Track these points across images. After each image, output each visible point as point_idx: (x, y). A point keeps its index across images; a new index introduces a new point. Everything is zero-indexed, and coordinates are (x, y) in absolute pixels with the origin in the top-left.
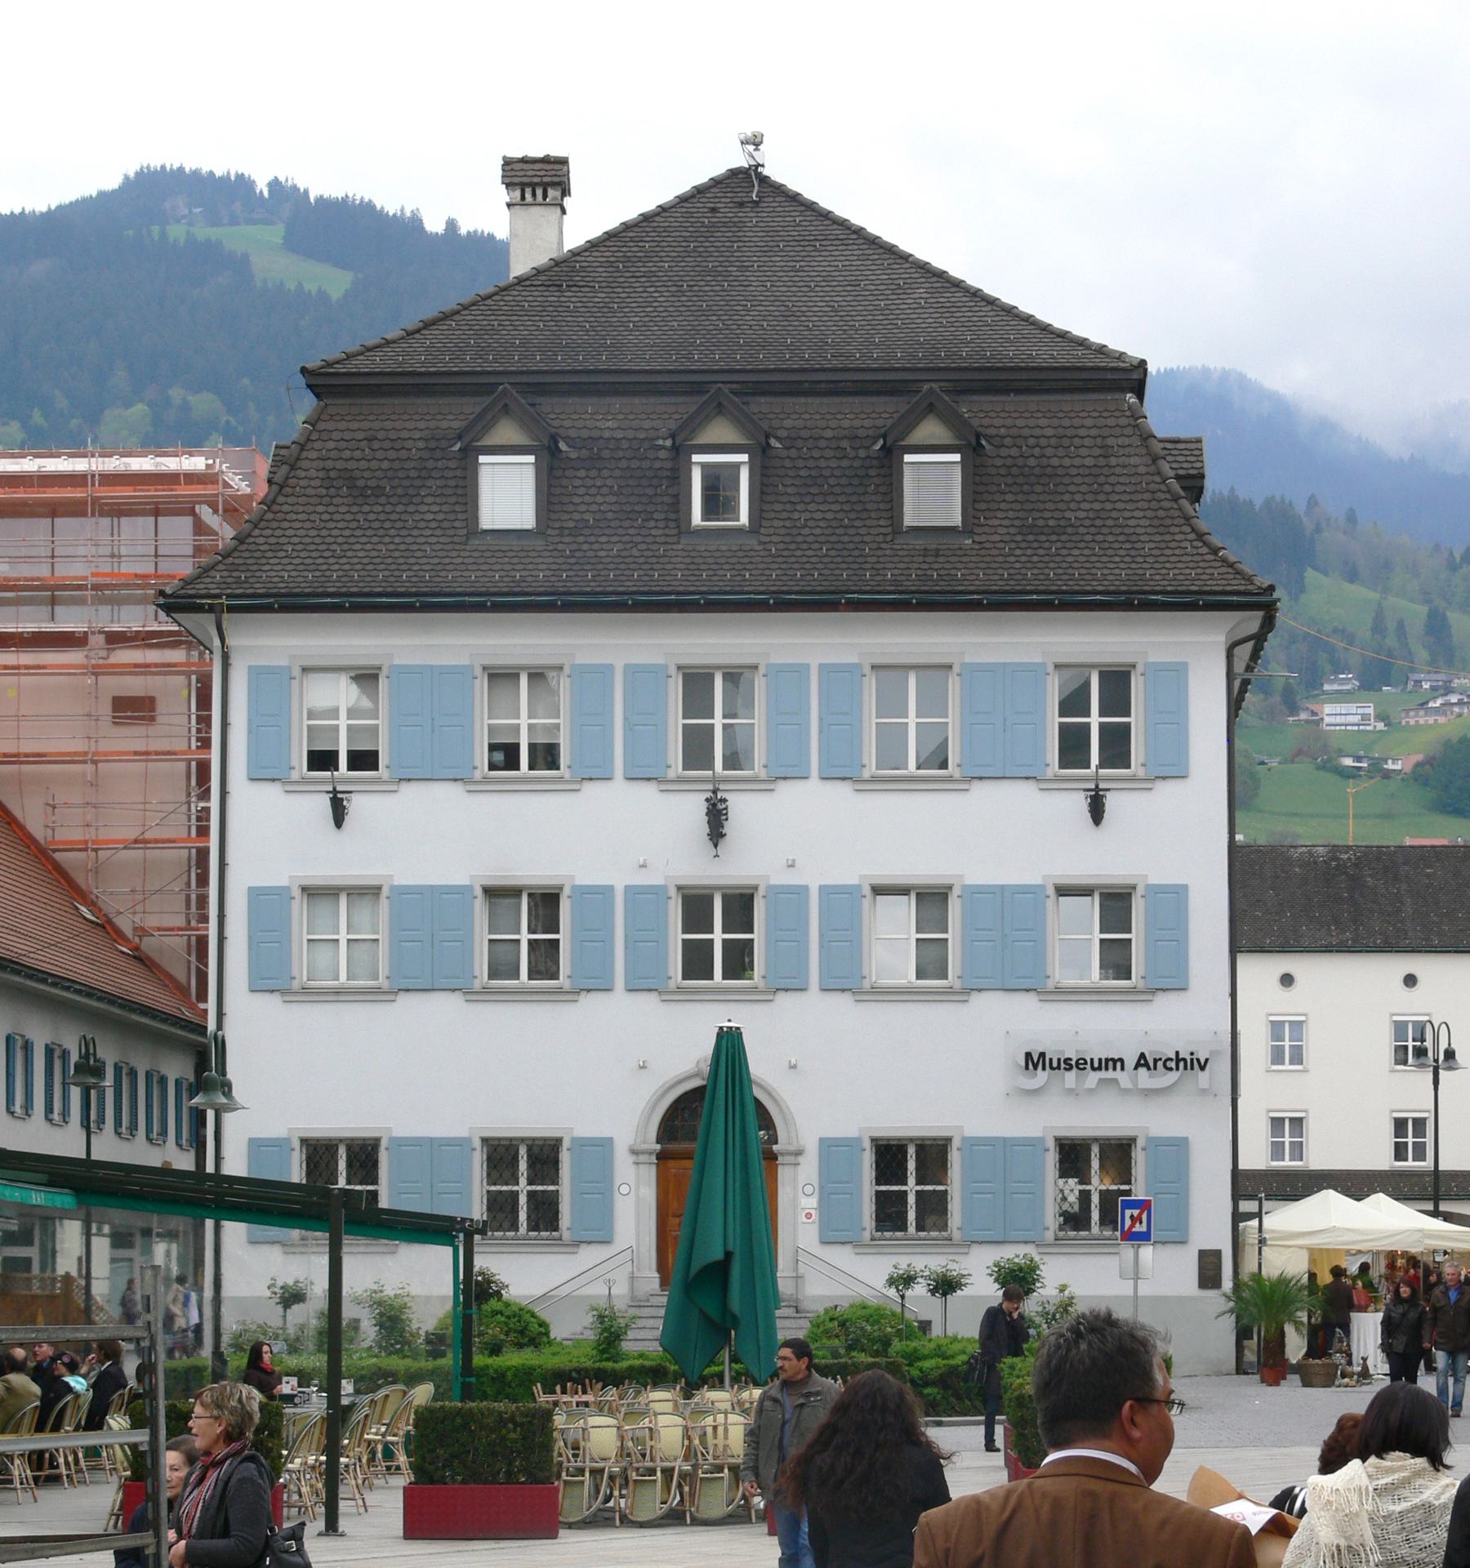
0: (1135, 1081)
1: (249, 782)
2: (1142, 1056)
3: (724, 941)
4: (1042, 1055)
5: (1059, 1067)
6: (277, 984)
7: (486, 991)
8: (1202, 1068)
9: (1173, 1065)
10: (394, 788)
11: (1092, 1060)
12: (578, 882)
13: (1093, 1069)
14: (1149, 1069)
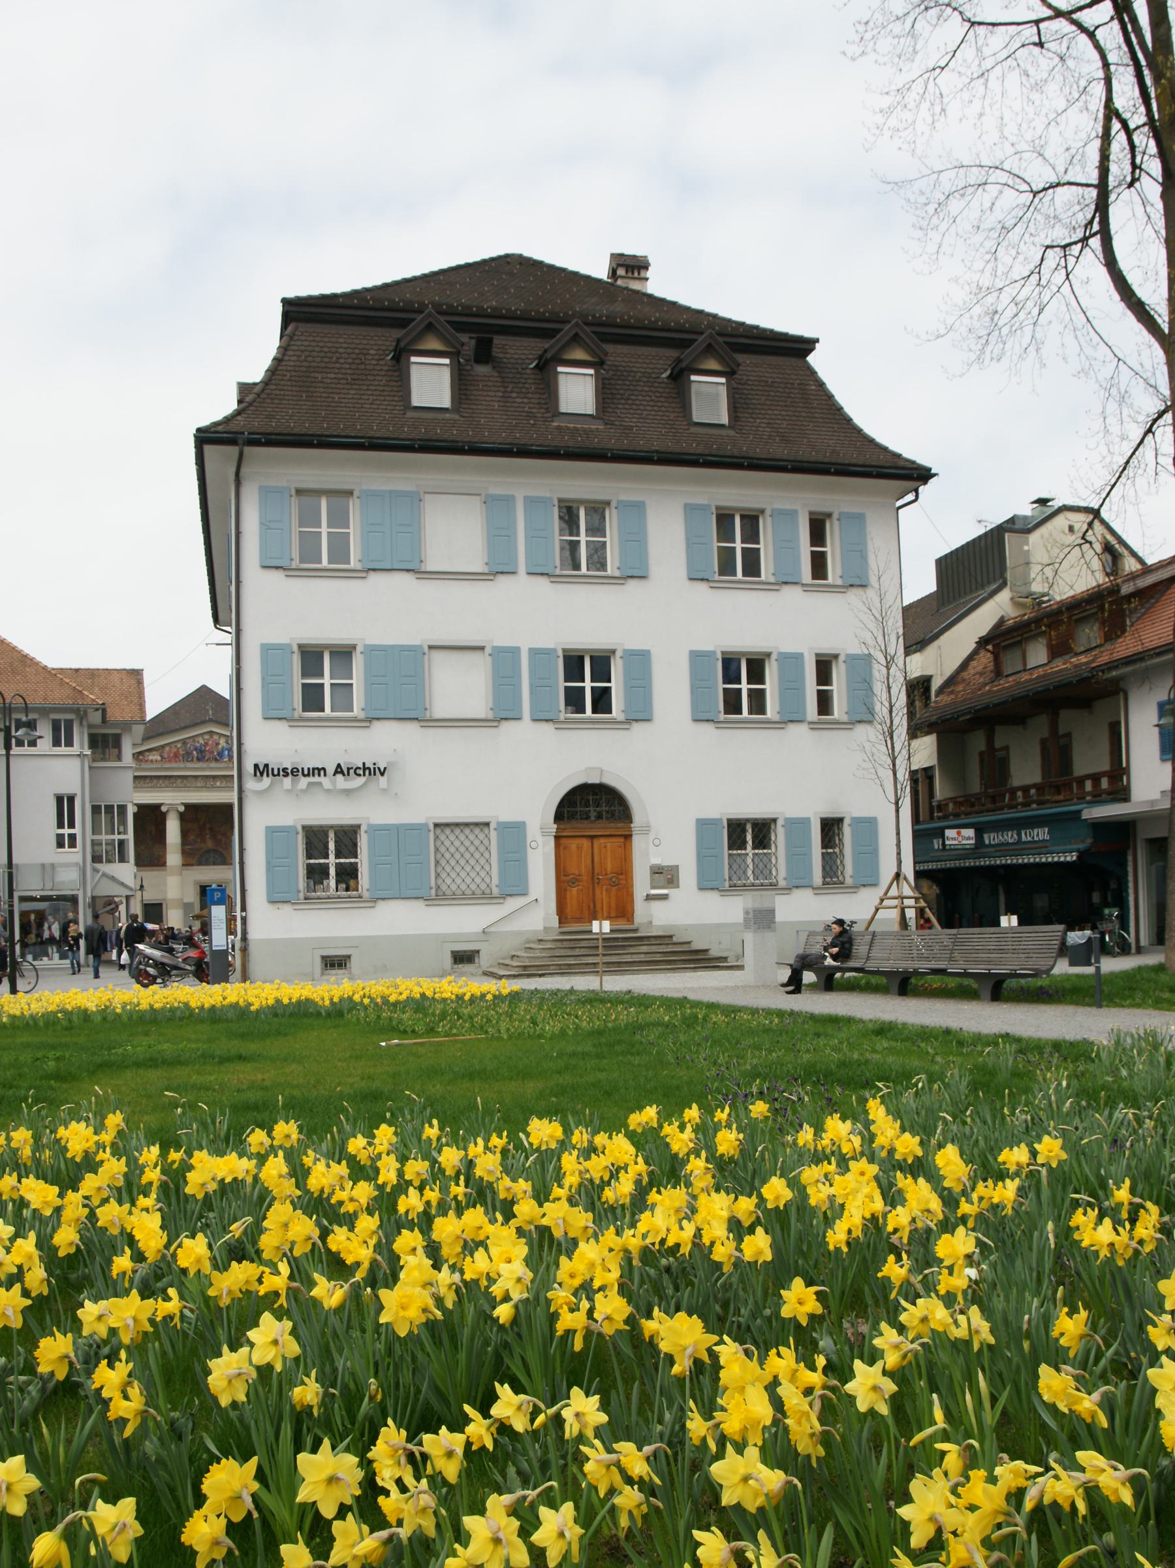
0: (334, 783)
1: (688, 583)
2: (339, 766)
3: (592, 688)
4: (266, 766)
5: (278, 774)
6: (288, 715)
7: (301, 719)
8: (382, 774)
9: (361, 772)
10: (364, 575)
12: (367, 642)
13: (304, 775)
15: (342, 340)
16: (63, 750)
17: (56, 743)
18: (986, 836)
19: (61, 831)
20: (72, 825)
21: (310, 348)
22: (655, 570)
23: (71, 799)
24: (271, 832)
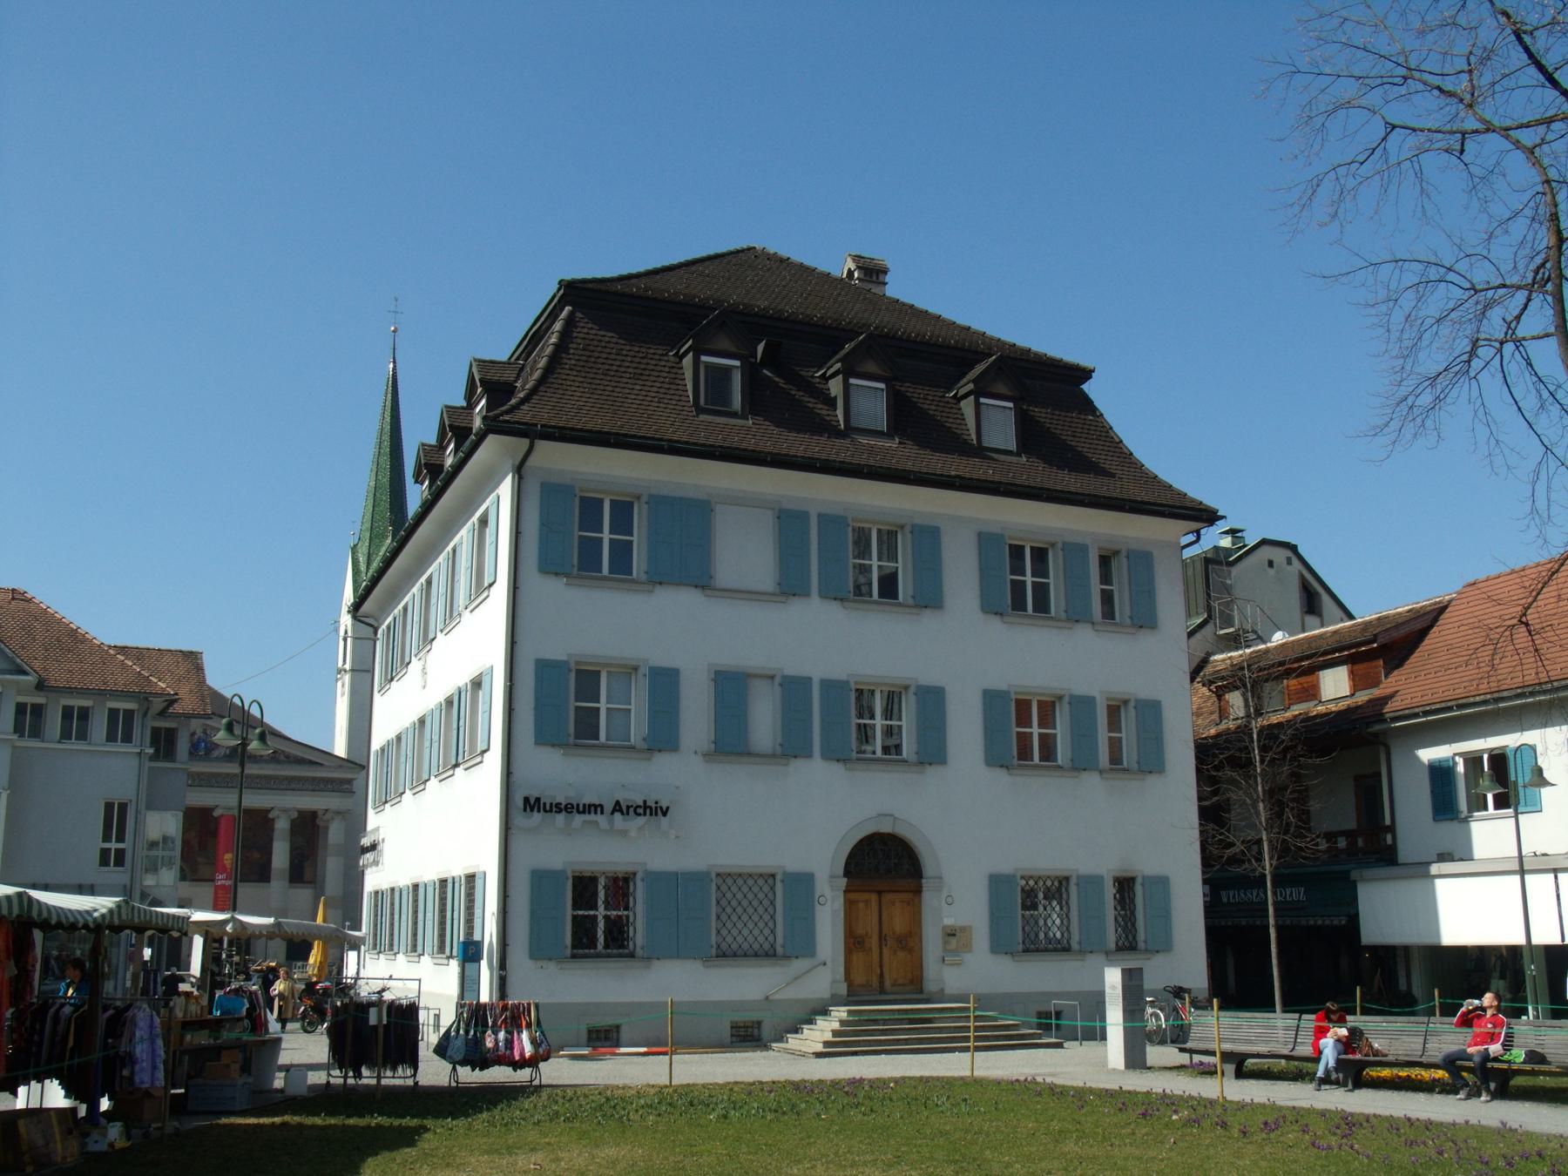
0: (611, 823)
2: (618, 803)
4: (538, 800)
8: (665, 814)
9: (640, 811)
11: (578, 805)
13: (579, 812)
14: (623, 814)
16: (119, 748)
18: (1223, 893)
19: (107, 845)
20: (120, 839)
22: (950, 599)
23: (123, 807)
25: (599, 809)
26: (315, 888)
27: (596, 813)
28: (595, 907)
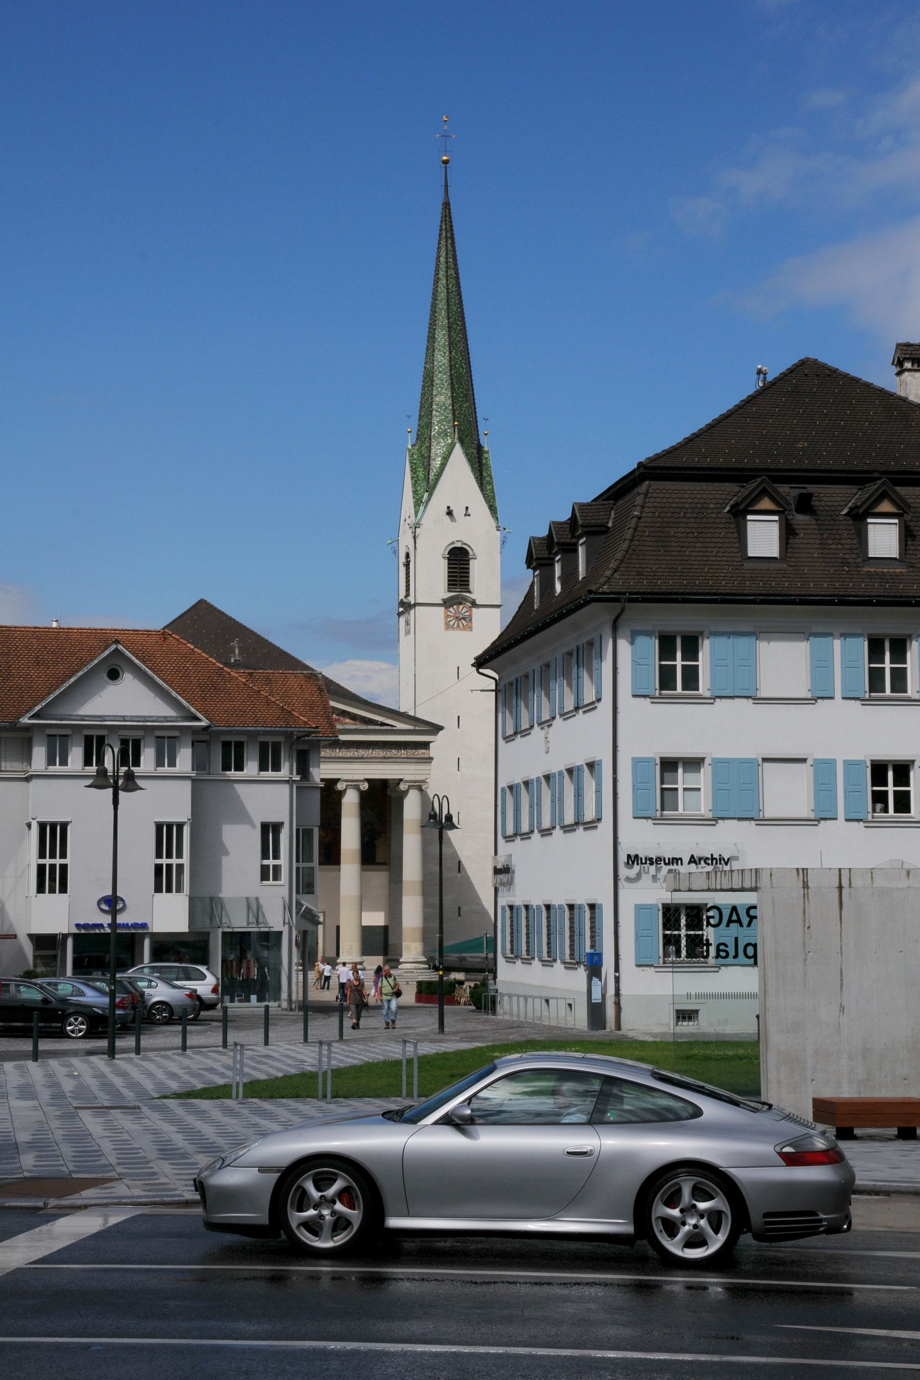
2: (692, 856)
3: (895, 792)
6: (653, 816)
9: (710, 862)
12: (714, 756)
13: (666, 864)
14: (696, 864)
15: (686, 496)
16: (270, 774)
17: (263, 767)
20: (276, 856)
21: (662, 505)
24: (639, 908)
25: (679, 862)
26: (389, 870)
27: (677, 864)
28: (679, 929)
